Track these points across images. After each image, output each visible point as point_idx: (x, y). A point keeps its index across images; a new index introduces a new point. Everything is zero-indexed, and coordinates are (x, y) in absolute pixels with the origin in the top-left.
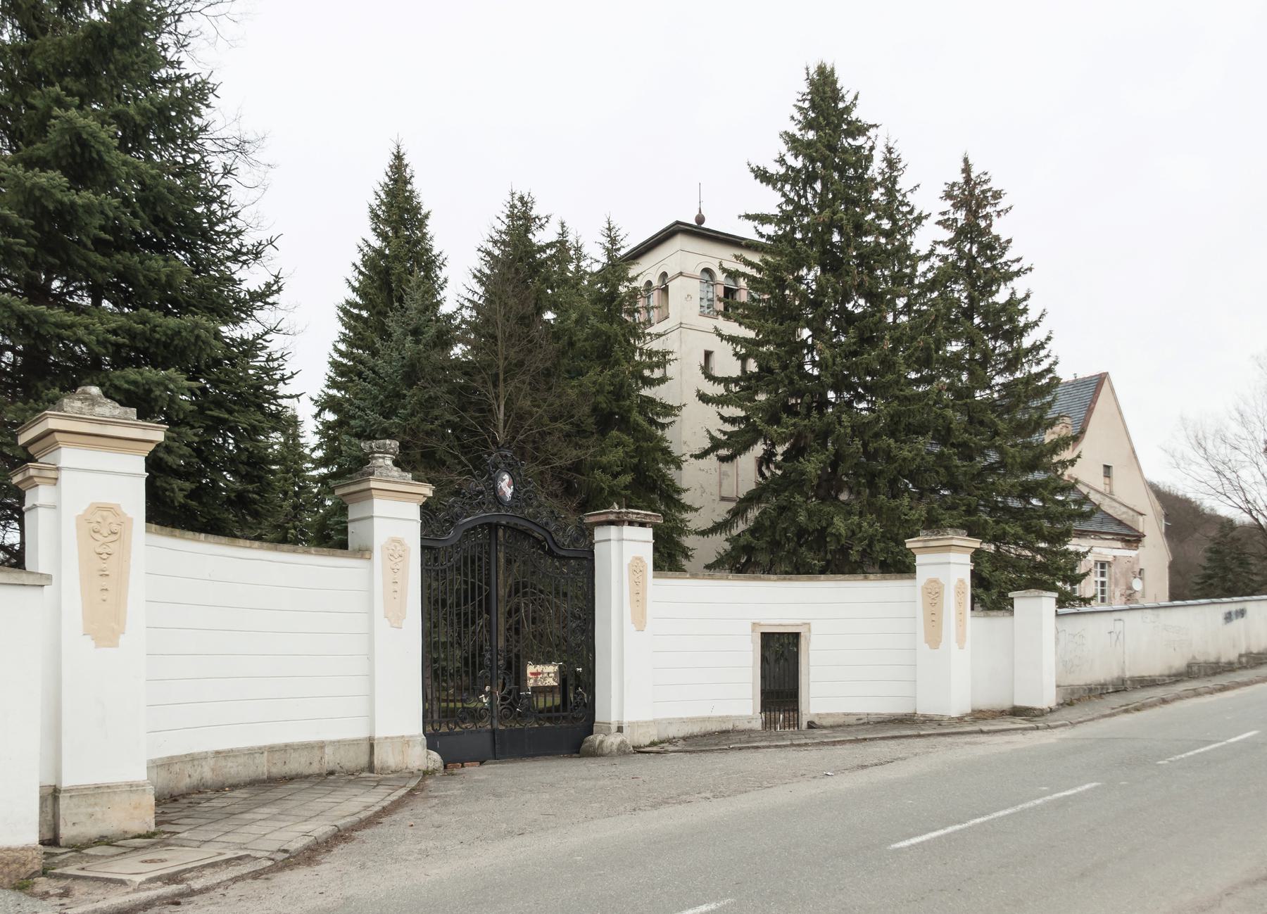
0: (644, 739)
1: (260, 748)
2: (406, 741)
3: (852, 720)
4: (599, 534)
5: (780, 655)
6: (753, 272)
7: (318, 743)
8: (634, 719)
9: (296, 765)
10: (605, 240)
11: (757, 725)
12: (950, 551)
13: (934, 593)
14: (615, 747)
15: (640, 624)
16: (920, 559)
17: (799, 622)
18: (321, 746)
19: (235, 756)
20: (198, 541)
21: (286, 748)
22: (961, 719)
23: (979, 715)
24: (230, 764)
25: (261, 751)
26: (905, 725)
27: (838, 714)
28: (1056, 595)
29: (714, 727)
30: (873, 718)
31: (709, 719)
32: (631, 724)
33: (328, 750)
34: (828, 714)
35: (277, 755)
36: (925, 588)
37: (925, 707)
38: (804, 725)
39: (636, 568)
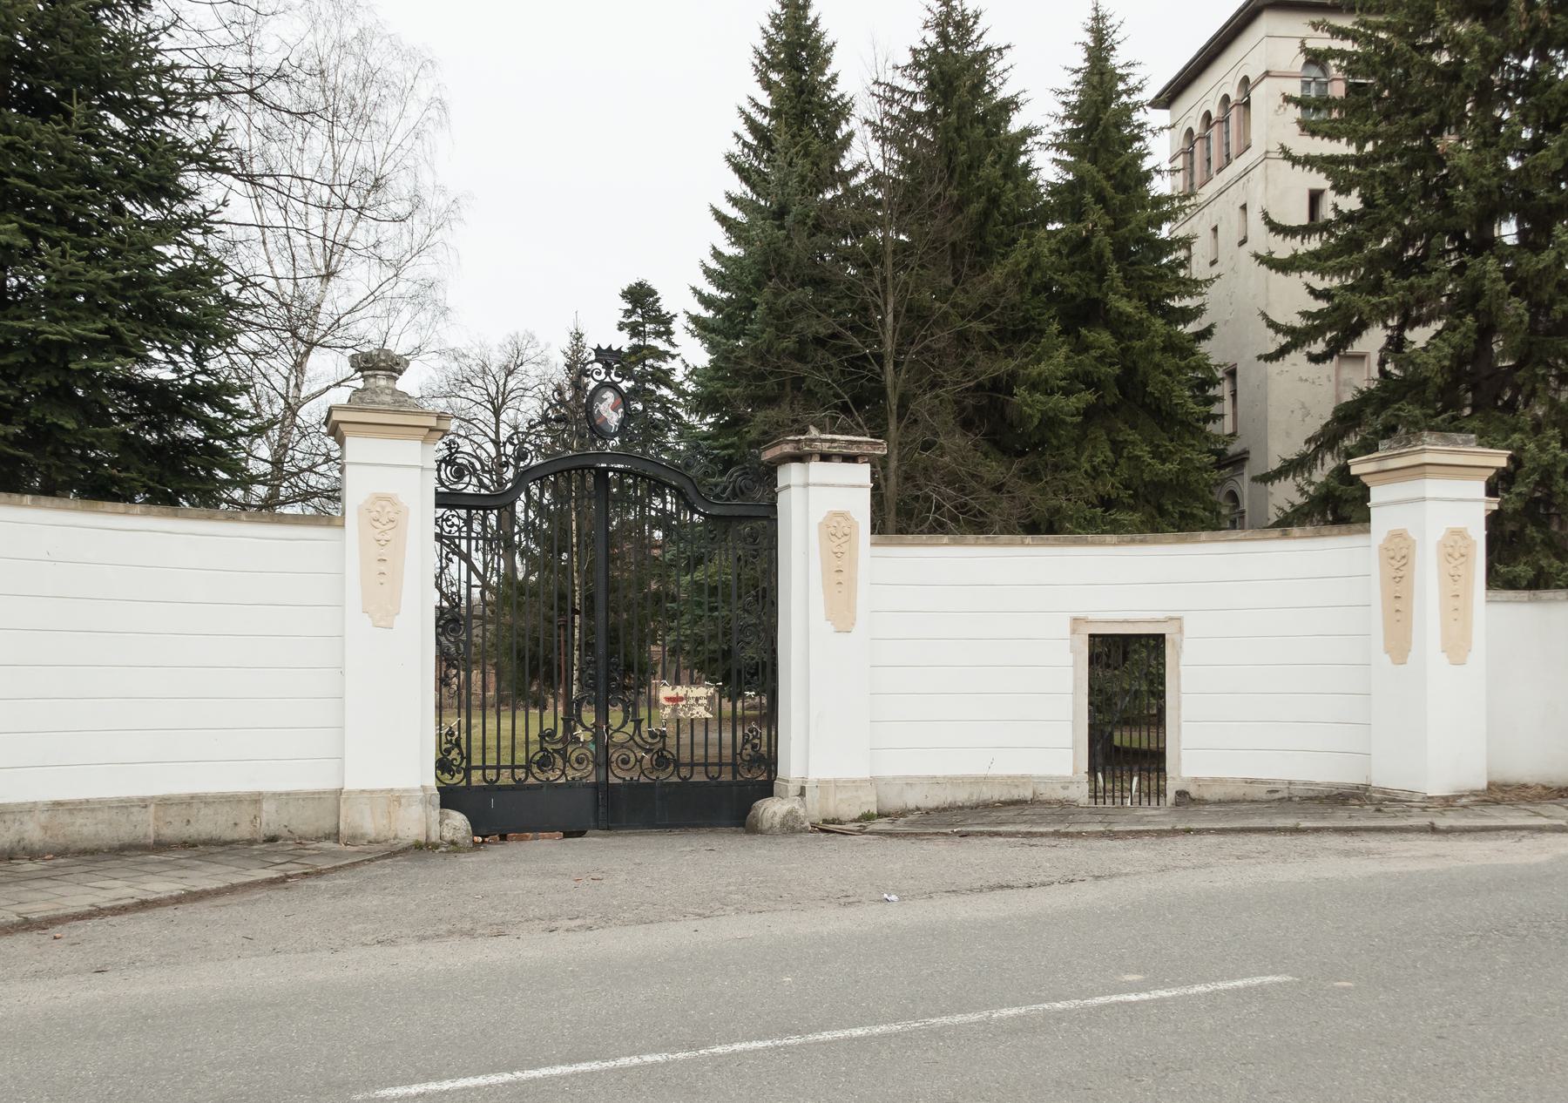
0: (849, 808)
1: (143, 800)
2: (395, 798)
3: (1260, 792)
4: (790, 475)
5: (1127, 680)
6: (1348, 46)
7: (251, 794)
8: (829, 775)
9: (206, 825)
10: (1088, 39)
11: (1080, 792)
12: (1423, 476)
13: (1399, 558)
14: (777, 820)
15: (843, 616)
16: (1377, 494)
17: (1161, 616)
18: (256, 799)
19: (93, 810)
20: (20, 505)
21: (190, 801)
22: (1448, 802)
23: (1499, 794)
24: (79, 821)
25: (144, 803)
26: (1344, 807)
27: (1234, 781)
28: (822, 498)
29: (962, 796)
30: (1298, 791)
31: (985, 780)
32: (822, 785)
33: (268, 808)
34: (1214, 780)
35: (173, 810)
36: (1384, 549)
37: (1385, 776)
38: (1171, 795)
39: (836, 529)
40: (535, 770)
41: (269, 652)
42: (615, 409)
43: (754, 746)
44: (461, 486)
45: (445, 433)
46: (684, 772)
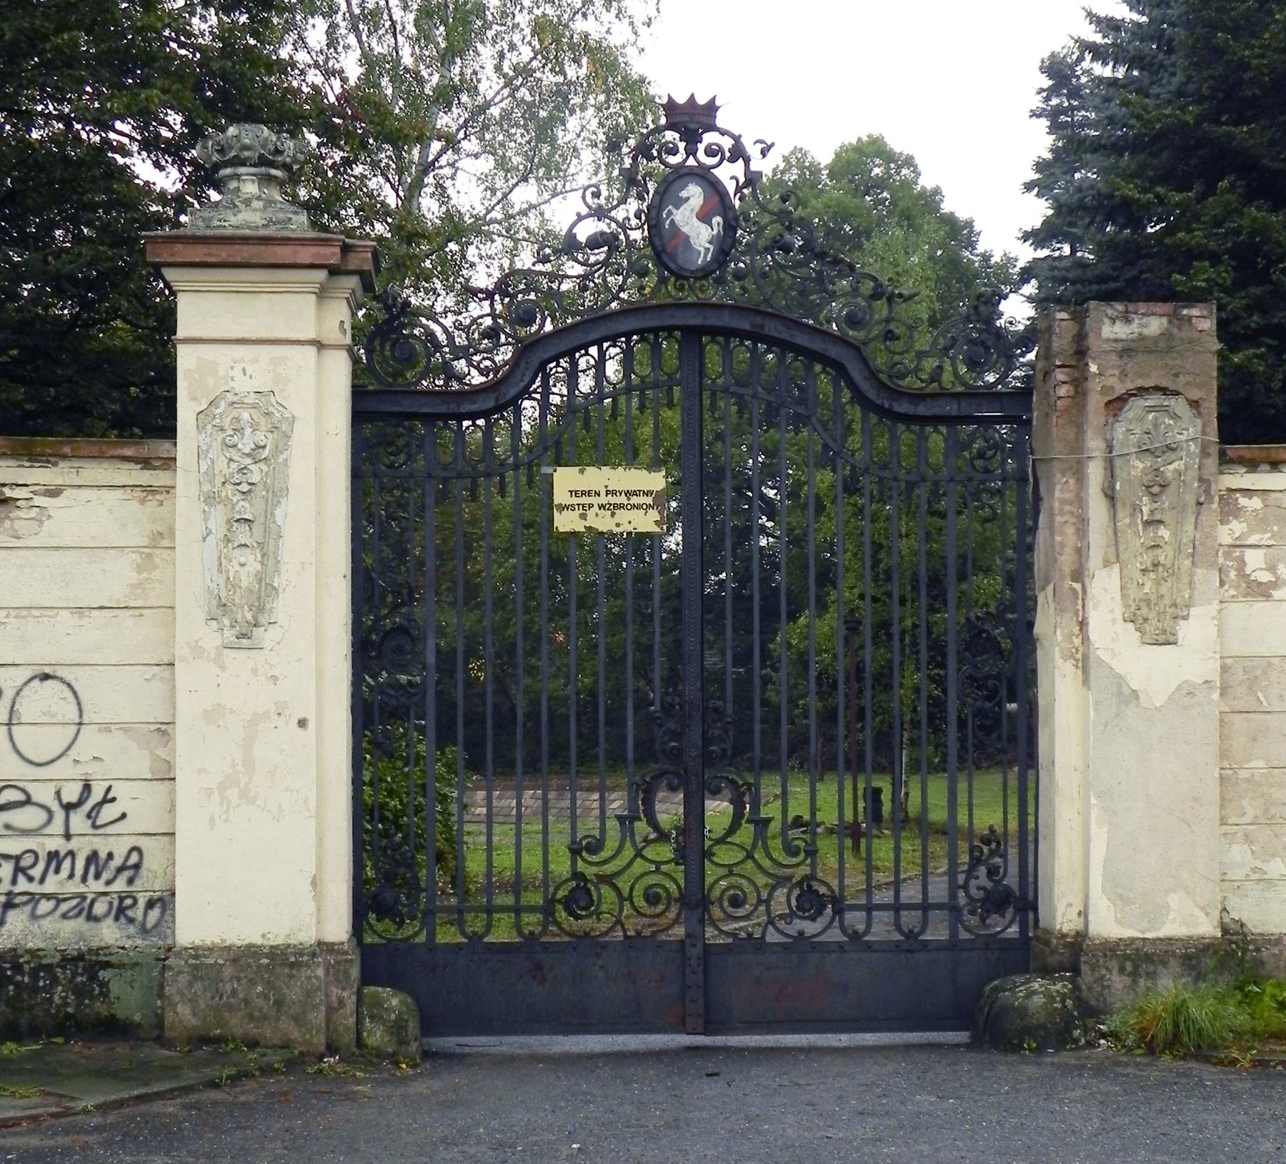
40: (561, 914)
41: (154, 677)
42: (704, 217)
43: (992, 872)
44: (535, 328)
45: (1261, 47)
46: (855, 919)
